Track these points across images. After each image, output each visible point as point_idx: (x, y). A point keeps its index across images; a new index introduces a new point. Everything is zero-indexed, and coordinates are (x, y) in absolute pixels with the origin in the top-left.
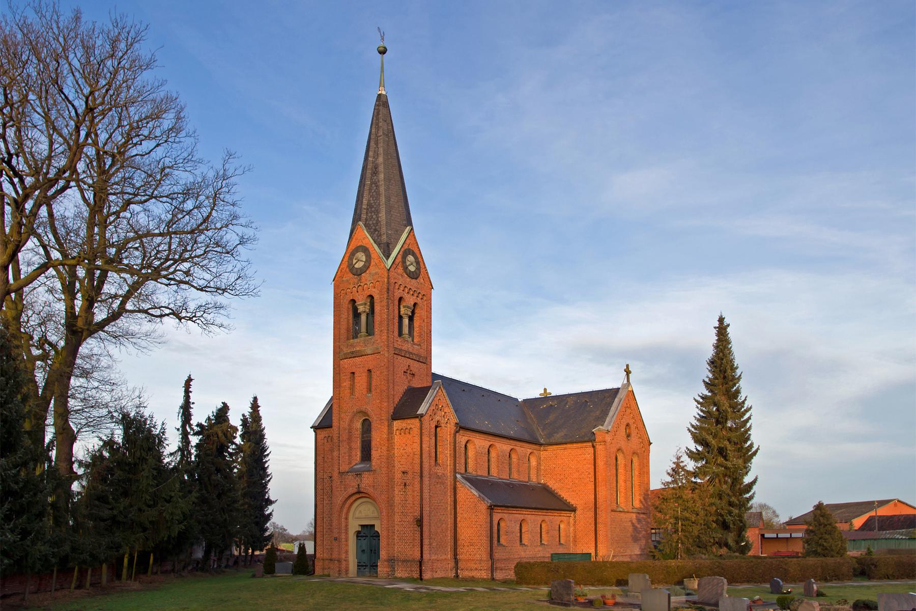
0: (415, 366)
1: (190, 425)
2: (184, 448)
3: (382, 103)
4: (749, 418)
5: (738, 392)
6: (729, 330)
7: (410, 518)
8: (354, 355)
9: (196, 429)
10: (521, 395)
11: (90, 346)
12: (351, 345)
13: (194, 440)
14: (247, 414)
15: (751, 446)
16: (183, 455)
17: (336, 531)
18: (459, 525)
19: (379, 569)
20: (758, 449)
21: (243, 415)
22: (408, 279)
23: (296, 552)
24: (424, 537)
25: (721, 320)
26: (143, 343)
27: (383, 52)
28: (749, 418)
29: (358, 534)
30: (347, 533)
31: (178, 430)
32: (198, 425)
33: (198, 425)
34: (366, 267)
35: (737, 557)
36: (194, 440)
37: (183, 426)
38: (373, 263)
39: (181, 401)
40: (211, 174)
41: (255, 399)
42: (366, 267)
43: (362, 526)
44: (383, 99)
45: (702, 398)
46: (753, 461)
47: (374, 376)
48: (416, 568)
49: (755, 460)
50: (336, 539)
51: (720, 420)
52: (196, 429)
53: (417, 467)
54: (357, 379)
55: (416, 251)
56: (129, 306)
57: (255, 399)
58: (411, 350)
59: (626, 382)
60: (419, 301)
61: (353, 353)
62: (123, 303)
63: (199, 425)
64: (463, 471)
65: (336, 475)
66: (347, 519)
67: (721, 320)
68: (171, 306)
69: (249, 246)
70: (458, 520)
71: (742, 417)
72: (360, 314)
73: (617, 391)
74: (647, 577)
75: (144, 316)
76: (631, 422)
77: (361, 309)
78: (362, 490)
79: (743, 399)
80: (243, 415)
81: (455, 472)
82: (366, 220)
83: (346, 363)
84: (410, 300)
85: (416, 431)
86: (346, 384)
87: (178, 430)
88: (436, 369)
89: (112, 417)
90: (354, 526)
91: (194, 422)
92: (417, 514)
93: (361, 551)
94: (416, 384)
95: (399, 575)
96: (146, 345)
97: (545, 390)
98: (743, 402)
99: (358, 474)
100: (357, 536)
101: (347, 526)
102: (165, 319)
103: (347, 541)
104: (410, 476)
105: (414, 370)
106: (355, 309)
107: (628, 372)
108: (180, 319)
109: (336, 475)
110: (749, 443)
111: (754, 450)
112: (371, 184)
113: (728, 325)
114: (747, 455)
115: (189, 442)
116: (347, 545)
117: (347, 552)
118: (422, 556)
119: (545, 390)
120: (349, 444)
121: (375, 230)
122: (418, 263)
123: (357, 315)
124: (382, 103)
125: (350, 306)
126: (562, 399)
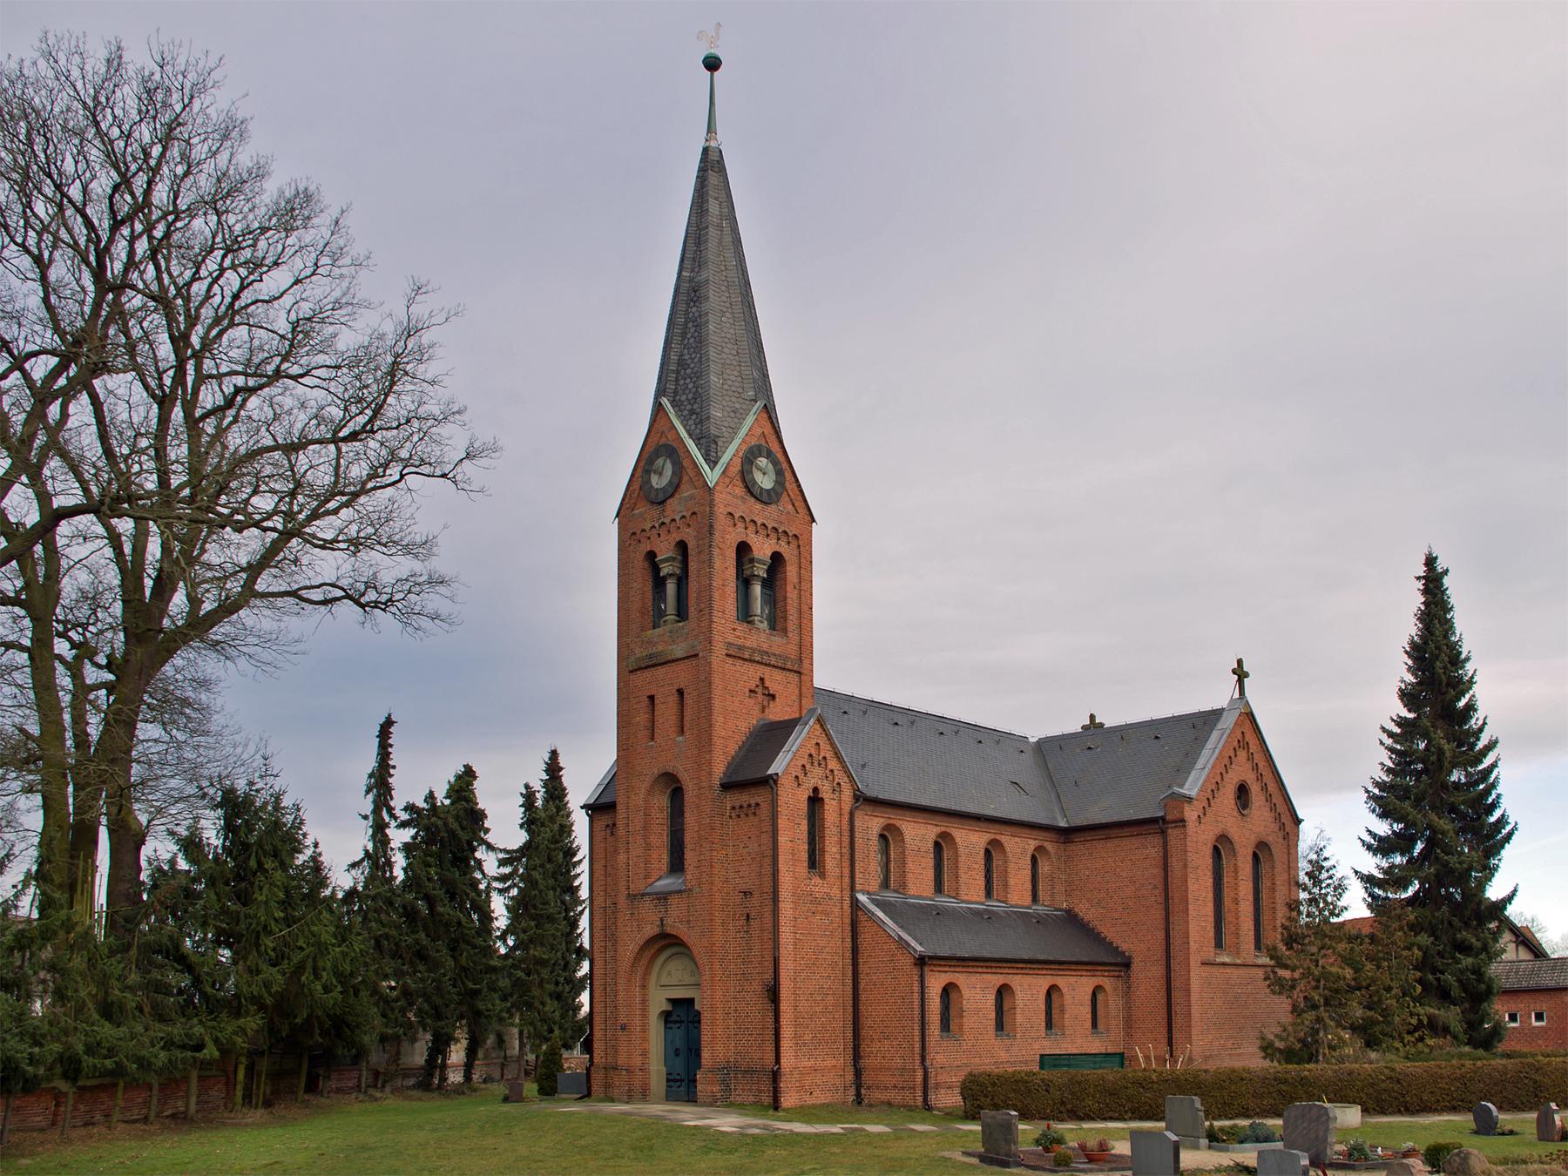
0: (775, 680)
1: (390, 810)
2: (377, 858)
3: (711, 165)
4: (1494, 765)
5: (1471, 708)
6: (1446, 581)
7: (756, 986)
8: (655, 663)
9: (404, 816)
10: (1035, 732)
11: (181, 666)
12: (649, 642)
13: (399, 837)
14: (537, 786)
15: (1502, 821)
16: (375, 866)
17: (623, 1010)
18: (863, 997)
19: (699, 1087)
20: (1515, 828)
21: (527, 786)
22: (759, 506)
23: (216, 1054)
24: (784, 1021)
25: (1430, 561)
26: (266, 655)
27: (712, 64)
28: (1494, 765)
29: (666, 1016)
30: (644, 1015)
31: (365, 817)
32: (405, 809)
33: (405, 809)
34: (674, 488)
35: (1461, 1056)
36: (399, 837)
37: (377, 811)
38: (685, 478)
39: (370, 762)
40: (389, 328)
41: (554, 754)
42: (674, 488)
43: (671, 1001)
44: (713, 156)
45: (1398, 724)
46: (1503, 852)
47: (688, 700)
48: (766, 1085)
49: (1507, 852)
50: (624, 1028)
51: (1436, 765)
52: (404, 816)
53: (768, 887)
54: (659, 708)
55: (775, 448)
56: (261, 586)
57: (554, 754)
58: (765, 647)
59: (1237, 695)
60: (783, 548)
61: (650, 656)
62: (251, 581)
63: (410, 808)
64: (874, 885)
65: (622, 900)
66: (644, 987)
67: (1430, 561)
68: (344, 583)
69: (484, 462)
70: (862, 986)
71: (1481, 762)
72: (664, 579)
73: (1215, 715)
74: (1198, 1105)
75: (291, 600)
76: (1250, 778)
77: (665, 570)
78: (669, 930)
79: (1480, 722)
80: (527, 786)
81: (853, 889)
82: (675, 392)
83: (640, 679)
84: (763, 549)
85: (764, 811)
86: (641, 718)
87: (365, 817)
88: (823, 678)
89: (204, 796)
90: (658, 1002)
91: (398, 803)
92: (769, 976)
93: (672, 1052)
94: (779, 712)
95: (739, 1099)
96: (270, 659)
97: (1092, 717)
98: (1481, 730)
99: (663, 897)
100: (666, 1022)
101: (644, 1001)
102: (336, 607)
103: (644, 1030)
104: (755, 901)
105: (773, 687)
106: (655, 568)
107: (1240, 674)
108: (363, 606)
109: (622, 900)
110: (1497, 814)
111: (1508, 828)
112: (686, 323)
113: (1446, 572)
114: (1490, 838)
115: (389, 841)
116: (645, 1039)
117: (645, 1054)
118: (778, 1061)
119: (1092, 717)
120: (645, 837)
121: (692, 412)
122: (779, 473)
123: (659, 583)
124: (711, 165)
125: (646, 565)
126: (1124, 732)
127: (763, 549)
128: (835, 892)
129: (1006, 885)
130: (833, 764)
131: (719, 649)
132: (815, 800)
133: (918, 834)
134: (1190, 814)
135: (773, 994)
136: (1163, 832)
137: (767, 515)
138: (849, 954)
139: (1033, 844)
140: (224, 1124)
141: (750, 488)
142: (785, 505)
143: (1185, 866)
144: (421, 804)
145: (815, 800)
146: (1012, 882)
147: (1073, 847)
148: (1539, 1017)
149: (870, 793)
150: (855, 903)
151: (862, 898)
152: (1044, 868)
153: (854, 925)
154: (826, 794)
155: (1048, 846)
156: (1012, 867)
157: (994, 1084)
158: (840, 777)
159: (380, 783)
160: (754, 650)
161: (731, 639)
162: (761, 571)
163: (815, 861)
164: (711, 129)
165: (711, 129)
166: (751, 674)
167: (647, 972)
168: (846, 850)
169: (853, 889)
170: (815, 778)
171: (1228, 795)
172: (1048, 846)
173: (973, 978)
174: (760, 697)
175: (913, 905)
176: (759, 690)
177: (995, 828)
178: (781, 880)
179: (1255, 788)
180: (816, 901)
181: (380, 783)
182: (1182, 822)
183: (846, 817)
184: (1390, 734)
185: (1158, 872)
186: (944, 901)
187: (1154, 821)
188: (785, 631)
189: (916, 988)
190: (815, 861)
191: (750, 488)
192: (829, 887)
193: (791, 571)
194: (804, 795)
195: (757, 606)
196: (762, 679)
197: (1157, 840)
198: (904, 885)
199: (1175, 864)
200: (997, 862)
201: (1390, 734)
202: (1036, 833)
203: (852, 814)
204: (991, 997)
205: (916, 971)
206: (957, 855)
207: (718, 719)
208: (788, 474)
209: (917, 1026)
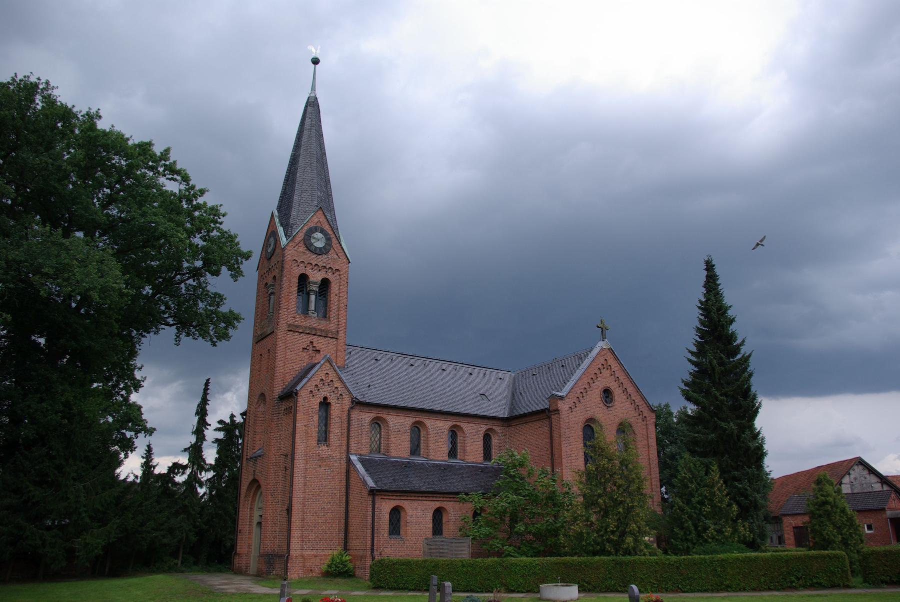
3: (312, 105)
22: (314, 256)
27: (316, 61)
60: (329, 276)
66: (251, 509)
84: (316, 277)
101: (251, 517)
116: (250, 538)
117: (249, 546)
124: (312, 105)
127: (316, 277)
128: (336, 454)
129: (464, 451)
130: (337, 384)
131: (283, 327)
132: (325, 404)
133: (438, 428)
134: (563, 406)
135: (289, 511)
136: (549, 418)
137: (321, 260)
138: (343, 489)
139: (484, 428)
140: (176, 572)
141: (309, 247)
142: (332, 255)
143: (560, 436)
144: (228, 421)
145: (325, 404)
146: (468, 449)
147: (511, 429)
148: (869, 528)
149: (362, 399)
150: (349, 461)
151: (354, 458)
152: (495, 441)
153: (348, 472)
154: (332, 399)
155: (496, 428)
156: (469, 441)
157: (463, 566)
158: (341, 390)
159: (202, 412)
160: (306, 328)
161: (292, 322)
162: (315, 288)
163: (324, 438)
164: (313, 88)
165: (313, 88)
166: (305, 340)
167: (253, 501)
168: (345, 431)
169: (348, 452)
170: (325, 392)
171: (596, 395)
172: (496, 428)
173: (416, 503)
174: (310, 352)
175: (392, 462)
176: (311, 348)
177: (454, 418)
178: (296, 447)
179: (617, 392)
180: (322, 459)
181: (202, 412)
182: (557, 411)
183: (346, 413)
184: (692, 353)
185: (548, 440)
186: (415, 459)
187: (543, 411)
188: (329, 319)
189: (370, 508)
190: (324, 438)
191: (309, 247)
192: (334, 451)
193: (334, 288)
194: (316, 401)
195: (312, 306)
196: (311, 342)
197: (546, 422)
198: (388, 451)
199: (555, 436)
200: (460, 438)
201: (692, 353)
202: (486, 421)
203: (349, 411)
204: (429, 516)
205: (370, 498)
206: (428, 433)
207: (279, 363)
208: (334, 240)
209: (369, 531)
